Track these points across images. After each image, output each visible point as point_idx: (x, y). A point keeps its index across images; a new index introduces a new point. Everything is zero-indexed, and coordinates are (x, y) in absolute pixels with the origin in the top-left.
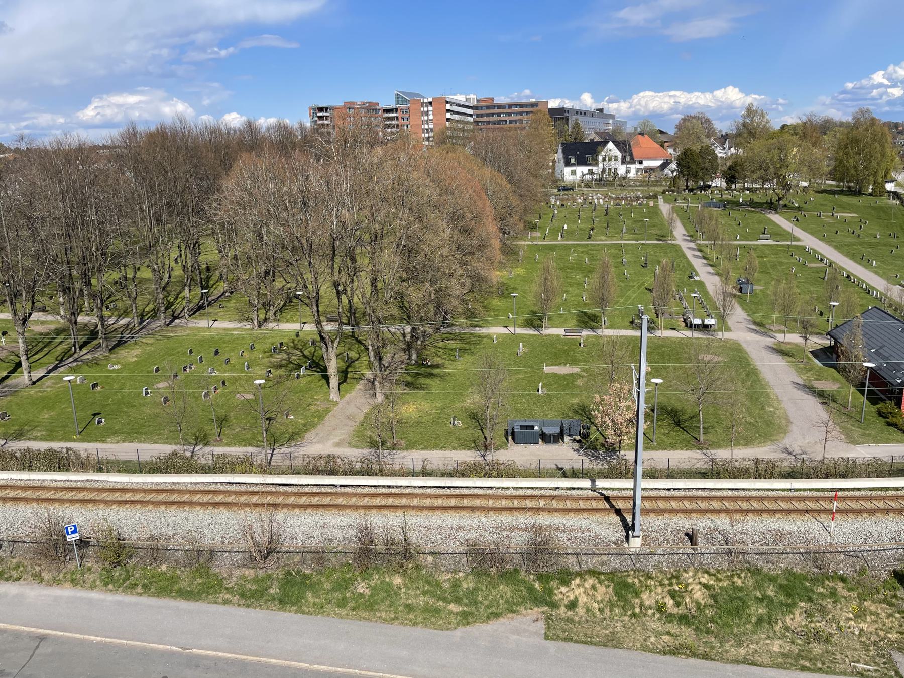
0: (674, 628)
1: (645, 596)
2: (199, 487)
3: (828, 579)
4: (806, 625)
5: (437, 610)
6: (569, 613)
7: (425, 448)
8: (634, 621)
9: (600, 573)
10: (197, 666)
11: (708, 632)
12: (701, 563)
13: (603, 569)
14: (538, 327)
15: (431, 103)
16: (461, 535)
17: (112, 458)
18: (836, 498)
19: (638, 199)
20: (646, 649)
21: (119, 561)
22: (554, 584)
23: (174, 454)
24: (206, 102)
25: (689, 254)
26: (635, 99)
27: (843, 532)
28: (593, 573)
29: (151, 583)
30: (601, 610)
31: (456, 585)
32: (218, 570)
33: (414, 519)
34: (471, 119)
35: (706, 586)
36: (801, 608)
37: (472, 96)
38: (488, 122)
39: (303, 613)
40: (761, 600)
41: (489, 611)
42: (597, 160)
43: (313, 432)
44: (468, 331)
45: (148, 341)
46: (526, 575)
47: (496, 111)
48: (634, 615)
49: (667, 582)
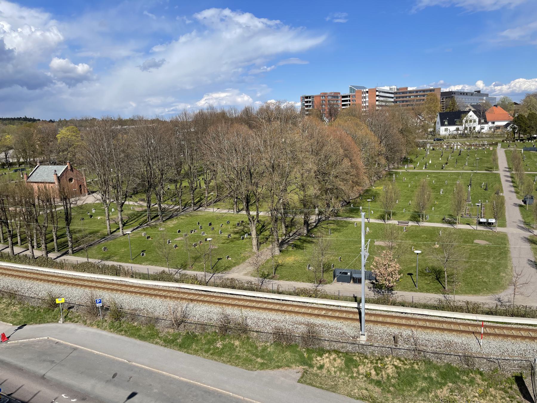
0: (371, 387)
1: (360, 368)
2: (8, 268)
3: (471, 372)
4: (448, 396)
5: (251, 360)
6: (318, 371)
7: (289, 280)
8: (351, 380)
9: (340, 352)
10: (132, 370)
11: (389, 391)
12: (397, 354)
13: (342, 350)
14: (418, 221)
15: (367, 92)
16: (274, 324)
17: (137, 271)
18: (482, 326)
19: (484, 145)
20: (349, 395)
21: (117, 319)
22: (314, 355)
23: (164, 272)
24: (259, 95)
25: (503, 179)
26: (513, 83)
27: (491, 347)
28: (337, 352)
29: (129, 330)
30: (335, 372)
31: (264, 349)
32: (158, 328)
33: (246, 312)
34: (393, 100)
35: (396, 367)
36: (448, 386)
37: (394, 87)
38: (403, 101)
39: (188, 353)
40: (425, 379)
41: (276, 364)
42: (462, 122)
43: (237, 267)
44: (345, 220)
45: (183, 217)
46: (301, 348)
47: (408, 94)
48: (352, 377)
49: (375, 362)
